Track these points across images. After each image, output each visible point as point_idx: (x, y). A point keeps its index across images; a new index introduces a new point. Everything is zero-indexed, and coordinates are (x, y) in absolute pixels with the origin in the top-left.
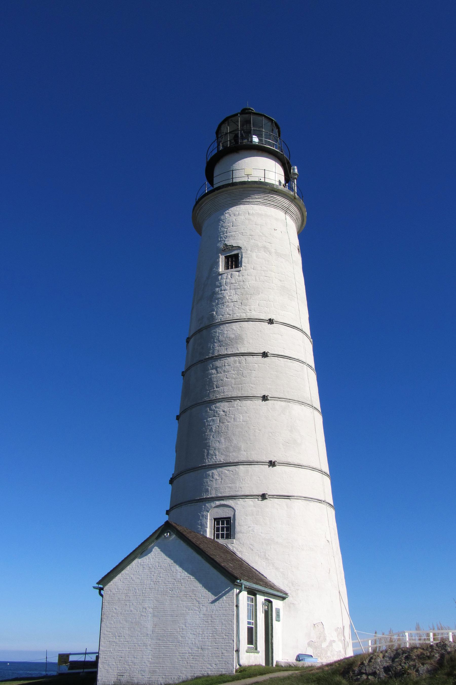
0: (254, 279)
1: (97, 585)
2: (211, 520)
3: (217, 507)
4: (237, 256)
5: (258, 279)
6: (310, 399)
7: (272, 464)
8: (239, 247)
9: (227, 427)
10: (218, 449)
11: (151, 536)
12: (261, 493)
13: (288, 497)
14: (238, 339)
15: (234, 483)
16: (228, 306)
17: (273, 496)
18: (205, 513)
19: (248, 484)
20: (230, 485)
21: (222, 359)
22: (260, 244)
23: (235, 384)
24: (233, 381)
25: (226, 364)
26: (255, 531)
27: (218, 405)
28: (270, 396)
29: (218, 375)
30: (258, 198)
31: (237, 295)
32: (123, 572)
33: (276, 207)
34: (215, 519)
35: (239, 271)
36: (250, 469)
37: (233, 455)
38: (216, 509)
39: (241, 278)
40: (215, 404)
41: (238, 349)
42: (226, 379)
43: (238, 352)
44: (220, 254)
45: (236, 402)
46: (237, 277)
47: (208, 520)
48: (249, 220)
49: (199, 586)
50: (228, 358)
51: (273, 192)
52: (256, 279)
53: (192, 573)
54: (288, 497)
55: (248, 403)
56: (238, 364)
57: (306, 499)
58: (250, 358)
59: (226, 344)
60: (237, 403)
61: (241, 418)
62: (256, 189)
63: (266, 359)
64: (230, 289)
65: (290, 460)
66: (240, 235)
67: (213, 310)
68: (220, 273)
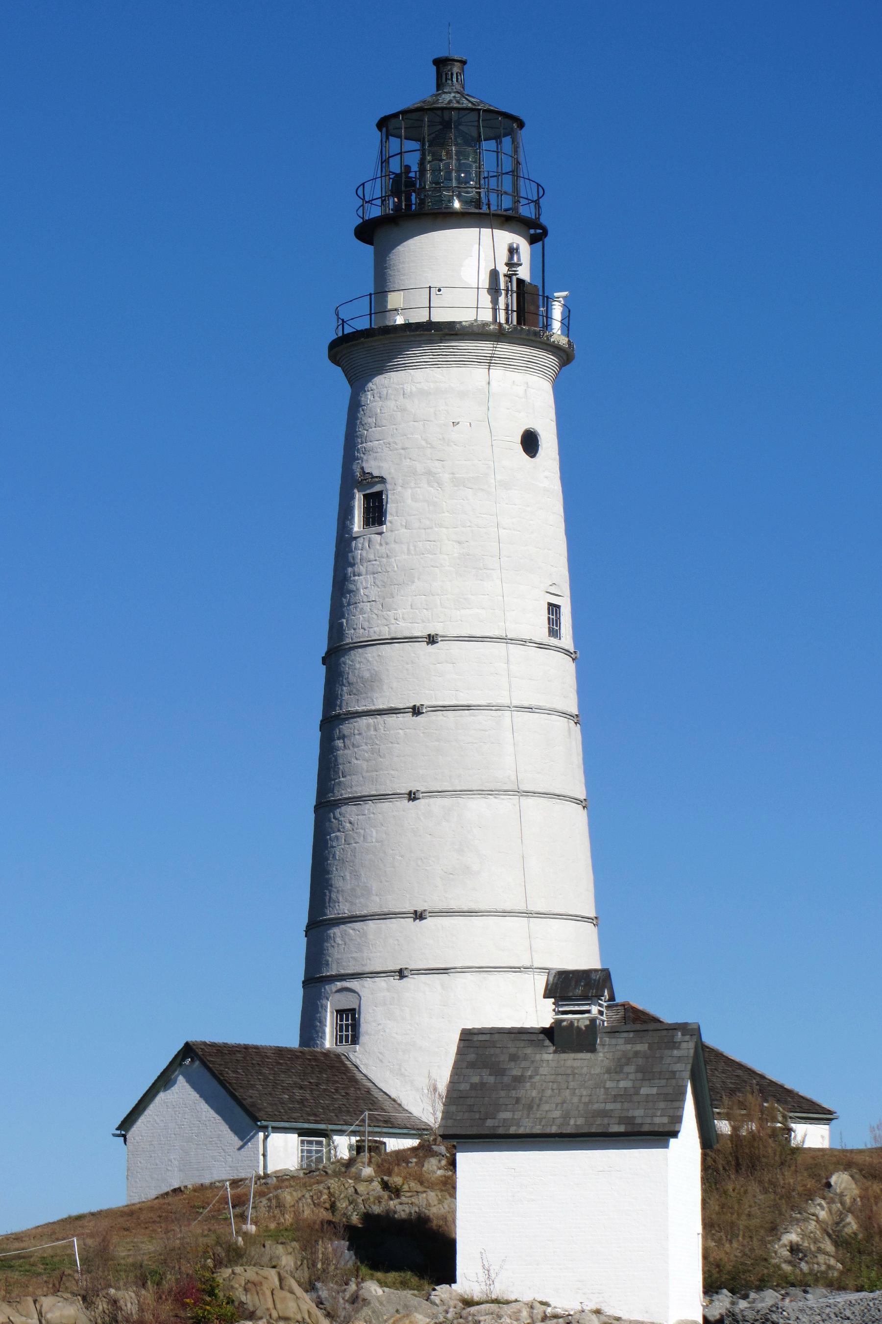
0: (406, 550)
1: (118, 1132)
2: (332, 1013)
3: (340, 990)
4: (379, 494)
5: (412, 548)
6: (513, 778)
7: (419, 916)
8: (382, 477)
9: (354, 851)
10: (343, 891)
11: (171, 1063)
12: (398, 968)
13: (445, 971)
14: (374, 681)
15: (361, 951)
16: (362, 612)
17: (419, 972)
18: (324, 1002)
19: (380, 952)
20: (355, 955)
21: (352, 721)
22: (420, 468)
23: (367, 771)
24: (365, 765)
25: (356, 732)
26: (387, 1030)
27: (344, 809)
28: (423, 790)
29: (346, 751)
30: (423, 353)
31: (376, 588)
32: (146, 1113)
33: (462, 363)
34: (338, 1011)
35: (380, 534)
36: (383, 926)
37: (360, 903)
38: (338, 996)
39: (383, 550)
40: (340, 807)
41: (373, 701)
42: (356, 762)
43: (373, 708)
44: (356, 491)
45: (367, 806)
46: (378, 547)
47: (329, 1014)
48: (404, 410)
49: (224, 1128)
50: (358, 719)
51: (447, 337)
52: (408, 550)
53: (218, 1112)
54: (445, 971)
55: (385, 806)
56: (372, 732)
57: (481, 969)
58: (391, 719)
59: (358, 690)
60: (369, 806)
61: (374, 833)
62: (413, 339)
63: (419, 718)
64: (367, 574)
65: (454, 905)
66: (386, 449)
67: (343, 617)
68: (354, 536)
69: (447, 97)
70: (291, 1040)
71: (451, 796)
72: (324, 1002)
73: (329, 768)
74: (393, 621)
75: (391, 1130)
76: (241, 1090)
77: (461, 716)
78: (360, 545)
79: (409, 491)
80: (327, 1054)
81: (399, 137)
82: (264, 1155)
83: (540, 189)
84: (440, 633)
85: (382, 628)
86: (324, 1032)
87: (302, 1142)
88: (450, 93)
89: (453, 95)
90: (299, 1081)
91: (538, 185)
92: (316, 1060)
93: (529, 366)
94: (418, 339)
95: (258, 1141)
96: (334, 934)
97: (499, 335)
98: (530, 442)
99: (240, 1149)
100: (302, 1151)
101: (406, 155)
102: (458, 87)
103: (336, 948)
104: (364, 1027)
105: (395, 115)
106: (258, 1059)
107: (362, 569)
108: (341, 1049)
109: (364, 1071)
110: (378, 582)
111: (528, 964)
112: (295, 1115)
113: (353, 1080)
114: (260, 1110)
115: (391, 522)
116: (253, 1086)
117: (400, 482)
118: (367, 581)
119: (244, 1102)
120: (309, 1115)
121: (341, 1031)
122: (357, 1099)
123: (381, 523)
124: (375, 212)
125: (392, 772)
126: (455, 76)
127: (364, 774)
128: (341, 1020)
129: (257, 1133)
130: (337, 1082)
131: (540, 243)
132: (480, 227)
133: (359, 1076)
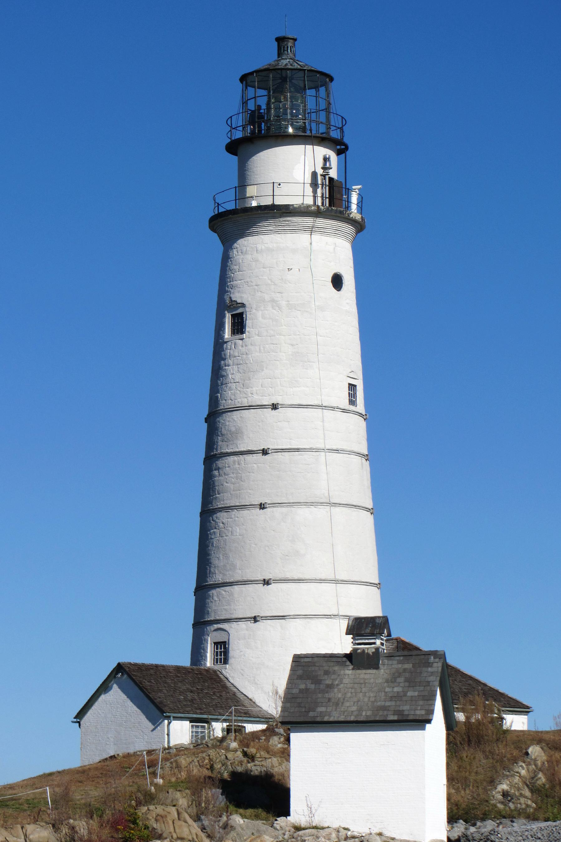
0: (258, 350)
1: (75, 720)
2: (211, 644)
3: (216, 630)
4: (241, 314)
5: (262, 348)
6: (327, 495)
7: (266, 582)
8: (243, 304)
9: (225, 541)
10: (218, 566)
11: (109, 676)
12: (253, 615)
13: (283, 617)
14: (238, 433)
15: (229, 605)
16: (230, 389)
17: (266, 618)
18: (206, 637)
19: (242, 605)
20: (226, 607)
21: (224, 458)
22: (267, 297)
23: (234, 491)
24: (232, 486)
25: (227, 465)
26: (246, 655)
27: (219, 514)
28: (269, 502)
29: (220, 478)
30: (269, 225)
31: (239, 374)
32: (93, 708)
33: (294, 231)
34: (215, 643)
35: (242, 339)
36: (244, 589)
37: (229, 574)
38: (215, 633)
39: (244, 350)
40: (216, 513)
41: (237, 446)
42: (226, 484)
43: (237, 450)
44: (226, 312)
45: (234, 513)
46: (240, 348)
47: (209, 645)
48: (257, 261)
49: (143, 718)
50: (228, 457)
51: (285, 215)
52: (260, 349)
53: (139, 707)
54: (283, 617)
55: (245, 512)
56: (237, 466)
57: (306, 616)
58: (249, 458)
59: (228, 439)
60: (235, 513)
61: (238, 530)
62: (263, 215)
63: (267, 457)
64: (233, 365)
65: (289, 576)
66: (245, 286)
67: (218, 392)
68: (225, 341)
69: (285, 62)
70: (185, 661)
71: (287, 506)
72: (206, 637)
73: (209, 489)
74: (250, 395)
75: (249, 719)
76: (153, 693)
77: (293, 455)
78: (229, 347)
79: (260, 312)
80: (208, 670)
81: (254, 87)
82: (168, 735)
83: (344, 120)
84: (280, 403)
85: (243, 400)
86: (206, 657)
87: (192, 726)
88: (286, 59)
89: (288, 60)
90: (190, 687)
91: (342, 118)
92: (201, 674)
93: (336, 233)
94: (266, 215)
95: (164, 726)
96: (213, 594)
97: (318, 213)
98: (337, 281)
99: (153, 730)
100: (192, 732)
101: (258, 99)
102: (291, 55)
103: (214, 603)
104: (231, 653)
105: (251, 73)
106: (164, 673)
107: (231, 362)
108: (217, 667)
109: (232, 681)
110: (240, 370)
111: (336, 613)
112: (188, 709)
113: (225, 687)
114: (165, 706)
115: (248, 332)
116: (161, 691)
117: (254, 306)
118: (233, 370)
119: (155, 701)
120: (196, 709)
121: (217, 656)
122: (227, 699)
123: (242, 333)
124: (239, 135)
125: (250, 491)
126: (289, 48)
127: (232, 492)
128: (217, 649)
129: (163, 721)
130: (214, 688)
131: (344, 155)
132: (305, 144)
133: (228, 684)
